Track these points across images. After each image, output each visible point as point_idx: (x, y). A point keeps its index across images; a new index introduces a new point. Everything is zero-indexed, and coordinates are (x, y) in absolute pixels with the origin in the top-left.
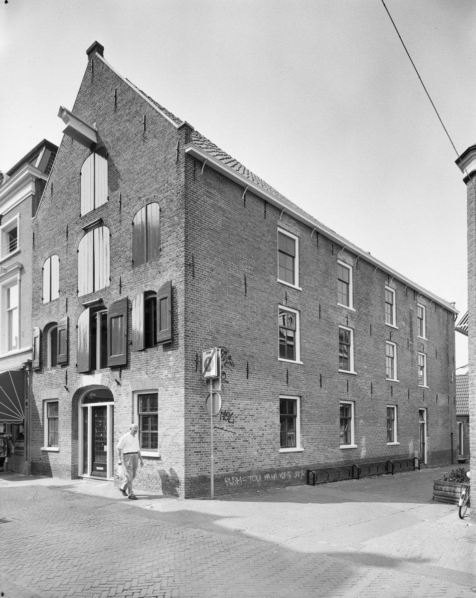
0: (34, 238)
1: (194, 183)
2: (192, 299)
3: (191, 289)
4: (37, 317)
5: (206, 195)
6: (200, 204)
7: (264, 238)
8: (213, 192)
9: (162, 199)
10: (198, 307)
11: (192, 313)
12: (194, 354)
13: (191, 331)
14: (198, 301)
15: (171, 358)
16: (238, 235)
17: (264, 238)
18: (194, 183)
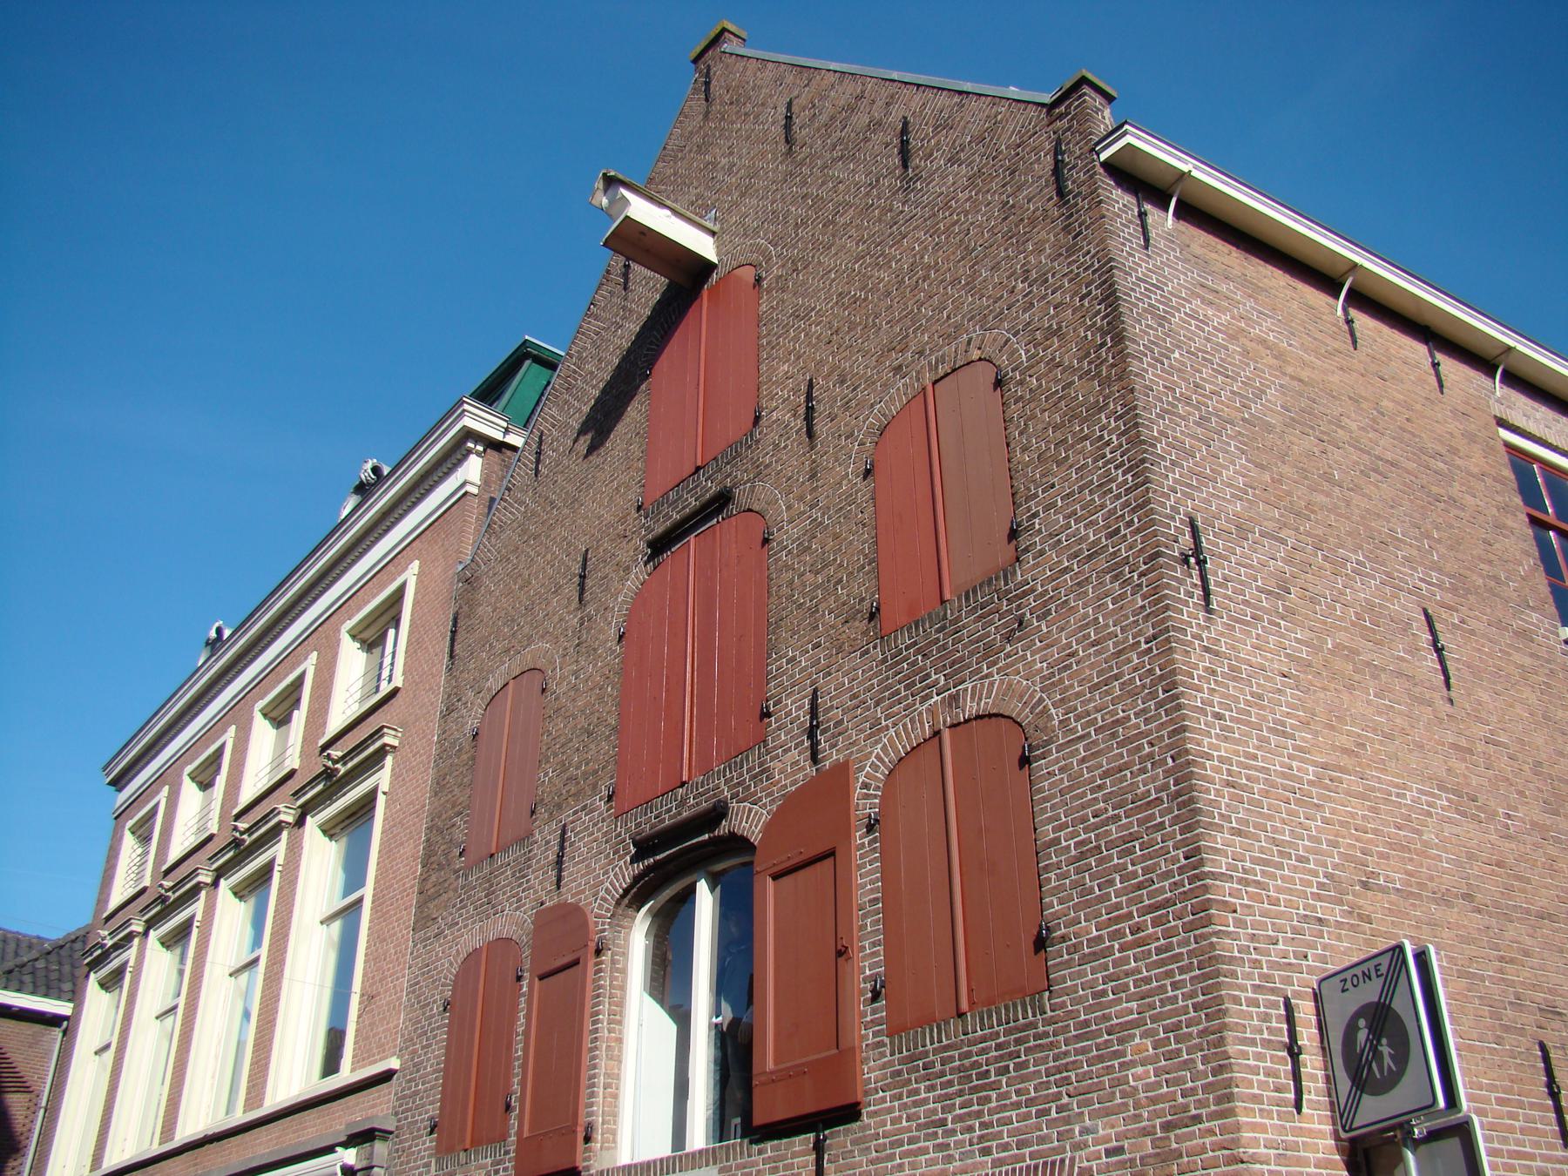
0: (454, 633)
1: (1148, 256)
2: (1218, 716)
3: (1206, 669)
4: (434, 929)
5: (1198, 296)
6: (1182, 327)
7: (1459, 462)
8: (1223, 288)
9: (1008, 340)
10: (1255, 757)
11: (1228, 784)
12: (1275, 1005)
13: (1240, 881)
14: (1248, 723)
15: (1139, 1041)
16: (1355, 447)
17: (1459, 462)
18: (1148, 256)
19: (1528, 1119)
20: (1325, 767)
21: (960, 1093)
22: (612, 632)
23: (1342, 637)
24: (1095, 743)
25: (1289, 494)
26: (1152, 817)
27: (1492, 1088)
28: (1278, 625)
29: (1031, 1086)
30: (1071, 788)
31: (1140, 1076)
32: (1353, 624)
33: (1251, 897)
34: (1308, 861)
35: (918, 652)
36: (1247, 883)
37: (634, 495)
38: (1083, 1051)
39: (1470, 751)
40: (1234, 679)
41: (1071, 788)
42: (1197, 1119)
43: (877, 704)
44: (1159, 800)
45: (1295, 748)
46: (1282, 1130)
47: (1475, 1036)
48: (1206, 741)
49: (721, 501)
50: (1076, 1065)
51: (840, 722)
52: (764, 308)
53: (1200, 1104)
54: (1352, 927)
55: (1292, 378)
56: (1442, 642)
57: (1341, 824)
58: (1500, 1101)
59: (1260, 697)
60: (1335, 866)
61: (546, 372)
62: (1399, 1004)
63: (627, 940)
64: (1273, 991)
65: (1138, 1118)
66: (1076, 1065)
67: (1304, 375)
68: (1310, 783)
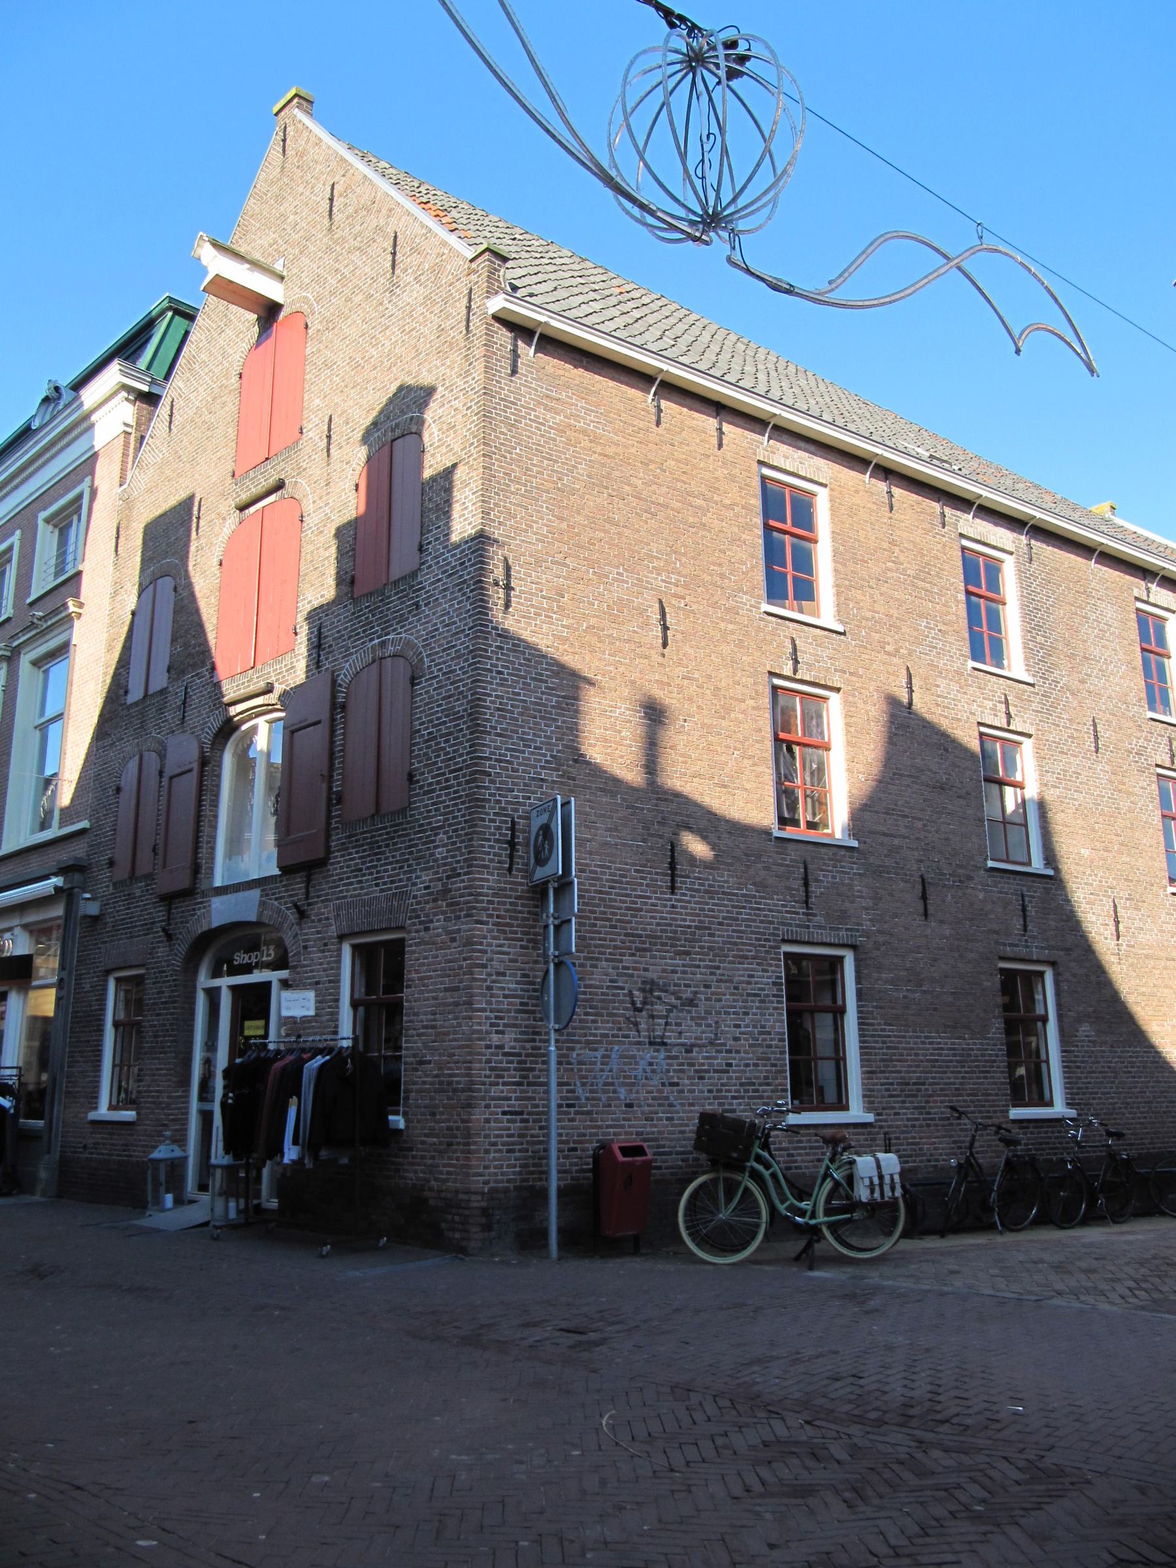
3: (497, 647)
5: (542, 404)
12: (506, 822)
13: (496, 760)
19: (651, 879)
20: (563, 697)
21: (369, 855)
22: (216, 562)
23: (593, 621)
24: (440, 681)
25: (578, 534)
26: (458, 725)
27: (634, 865)
28: (551, 617)
29: (397, 854)
30: (429, 703)
31: (440, 852)
32: (605, 613)
33: (501, 768)
34: (541, 749)
35: (370, 611)
36: (500, 761)
37: (230, 466)
38: (420, 838)
39: (669, 684)
40: (515, 651)
41: (429, 703)
42: (459, 875)
43: (349, 638)
44: (463, 717)
45: (547, 688)
46: (499, 882)
47: (629, 837)
48: (489, 687)
49: (280, 486)
50: (416, 845)
51: (331, 646)
52: (308, 351)
53: (462, 868)
54: (562, 783)
55: (600, 454)
56: (669, 620)
57: (568, 728)
58: (636, 871)
59: (529, 660)
60: (558, 751)
61: (185, 322)
62: (553, 826)
63: (221, 757)
64: (506, 815)
65: (437, 873)
66: (416, 845)
67: (611, 451)
68: (553, 707)
